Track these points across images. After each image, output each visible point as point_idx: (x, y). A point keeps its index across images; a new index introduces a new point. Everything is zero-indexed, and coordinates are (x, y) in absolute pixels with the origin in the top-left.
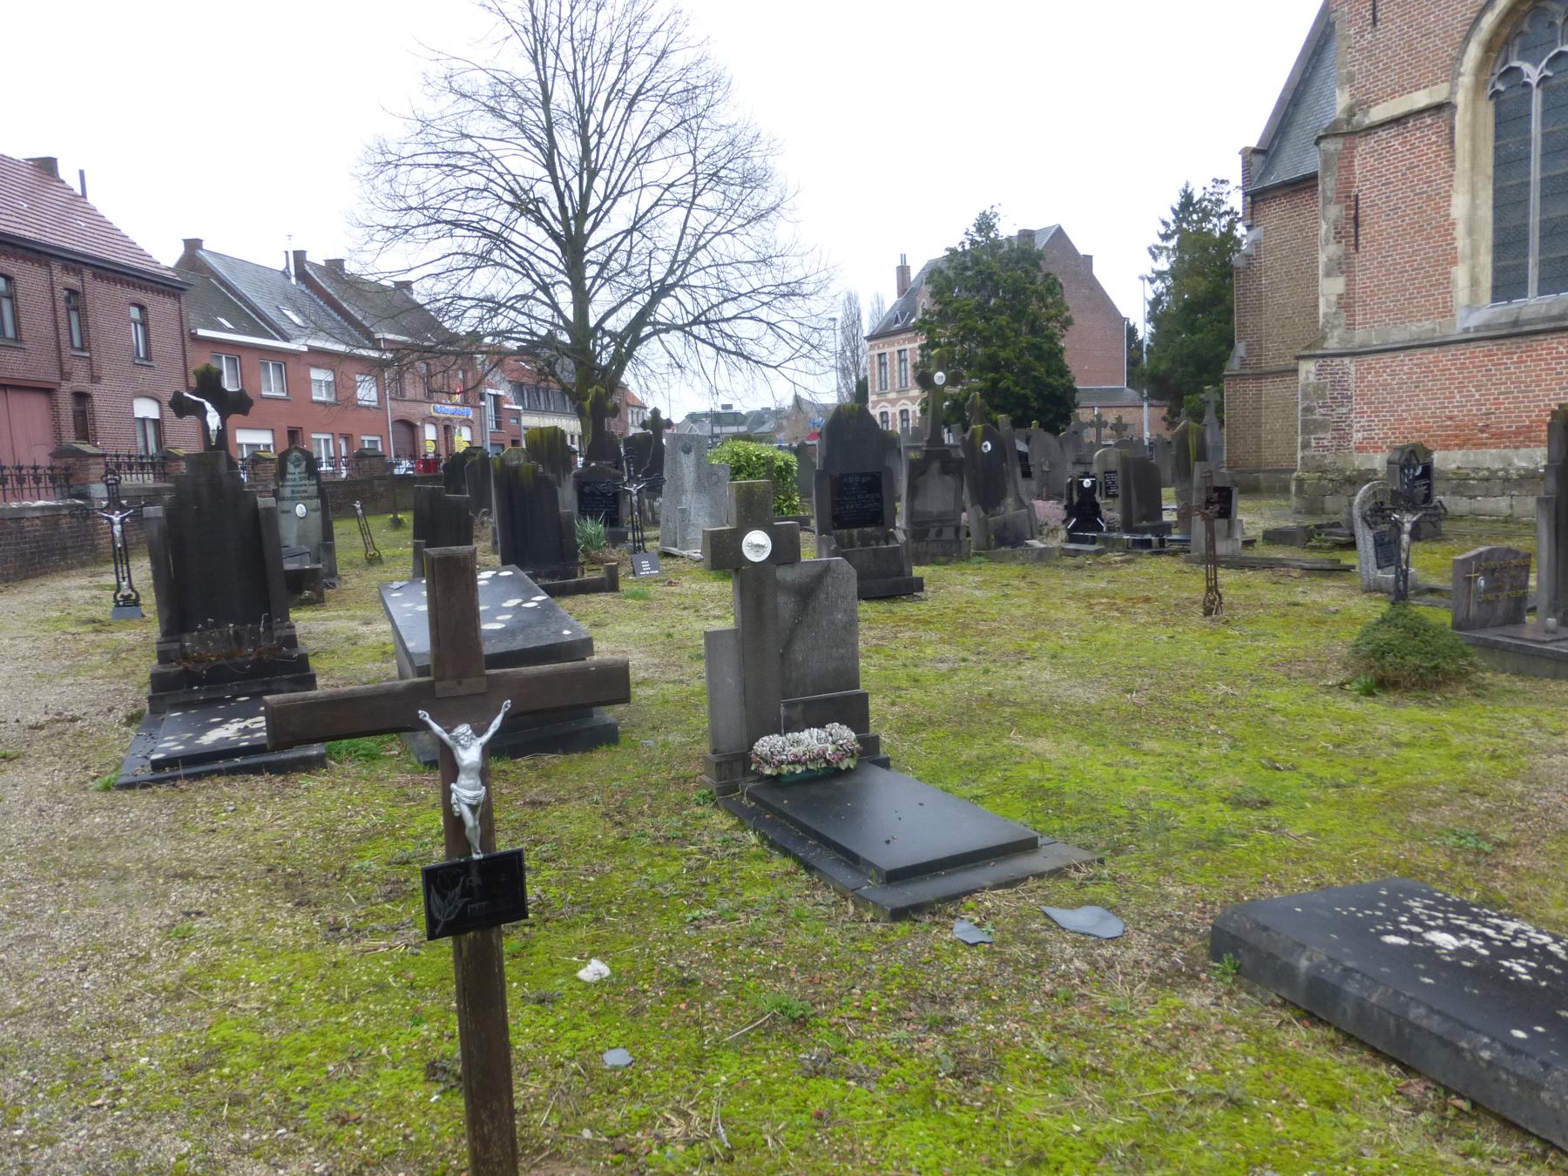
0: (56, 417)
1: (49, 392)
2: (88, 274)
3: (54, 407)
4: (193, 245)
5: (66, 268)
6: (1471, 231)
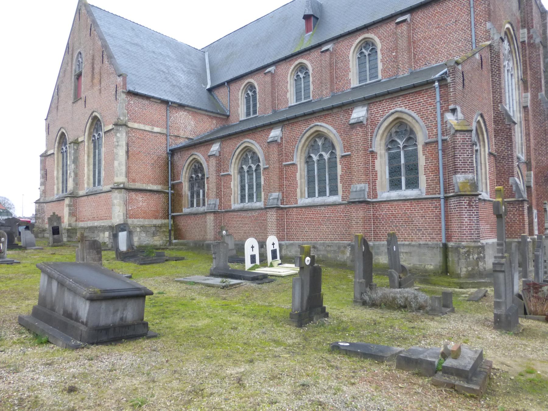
6: (57, 179)
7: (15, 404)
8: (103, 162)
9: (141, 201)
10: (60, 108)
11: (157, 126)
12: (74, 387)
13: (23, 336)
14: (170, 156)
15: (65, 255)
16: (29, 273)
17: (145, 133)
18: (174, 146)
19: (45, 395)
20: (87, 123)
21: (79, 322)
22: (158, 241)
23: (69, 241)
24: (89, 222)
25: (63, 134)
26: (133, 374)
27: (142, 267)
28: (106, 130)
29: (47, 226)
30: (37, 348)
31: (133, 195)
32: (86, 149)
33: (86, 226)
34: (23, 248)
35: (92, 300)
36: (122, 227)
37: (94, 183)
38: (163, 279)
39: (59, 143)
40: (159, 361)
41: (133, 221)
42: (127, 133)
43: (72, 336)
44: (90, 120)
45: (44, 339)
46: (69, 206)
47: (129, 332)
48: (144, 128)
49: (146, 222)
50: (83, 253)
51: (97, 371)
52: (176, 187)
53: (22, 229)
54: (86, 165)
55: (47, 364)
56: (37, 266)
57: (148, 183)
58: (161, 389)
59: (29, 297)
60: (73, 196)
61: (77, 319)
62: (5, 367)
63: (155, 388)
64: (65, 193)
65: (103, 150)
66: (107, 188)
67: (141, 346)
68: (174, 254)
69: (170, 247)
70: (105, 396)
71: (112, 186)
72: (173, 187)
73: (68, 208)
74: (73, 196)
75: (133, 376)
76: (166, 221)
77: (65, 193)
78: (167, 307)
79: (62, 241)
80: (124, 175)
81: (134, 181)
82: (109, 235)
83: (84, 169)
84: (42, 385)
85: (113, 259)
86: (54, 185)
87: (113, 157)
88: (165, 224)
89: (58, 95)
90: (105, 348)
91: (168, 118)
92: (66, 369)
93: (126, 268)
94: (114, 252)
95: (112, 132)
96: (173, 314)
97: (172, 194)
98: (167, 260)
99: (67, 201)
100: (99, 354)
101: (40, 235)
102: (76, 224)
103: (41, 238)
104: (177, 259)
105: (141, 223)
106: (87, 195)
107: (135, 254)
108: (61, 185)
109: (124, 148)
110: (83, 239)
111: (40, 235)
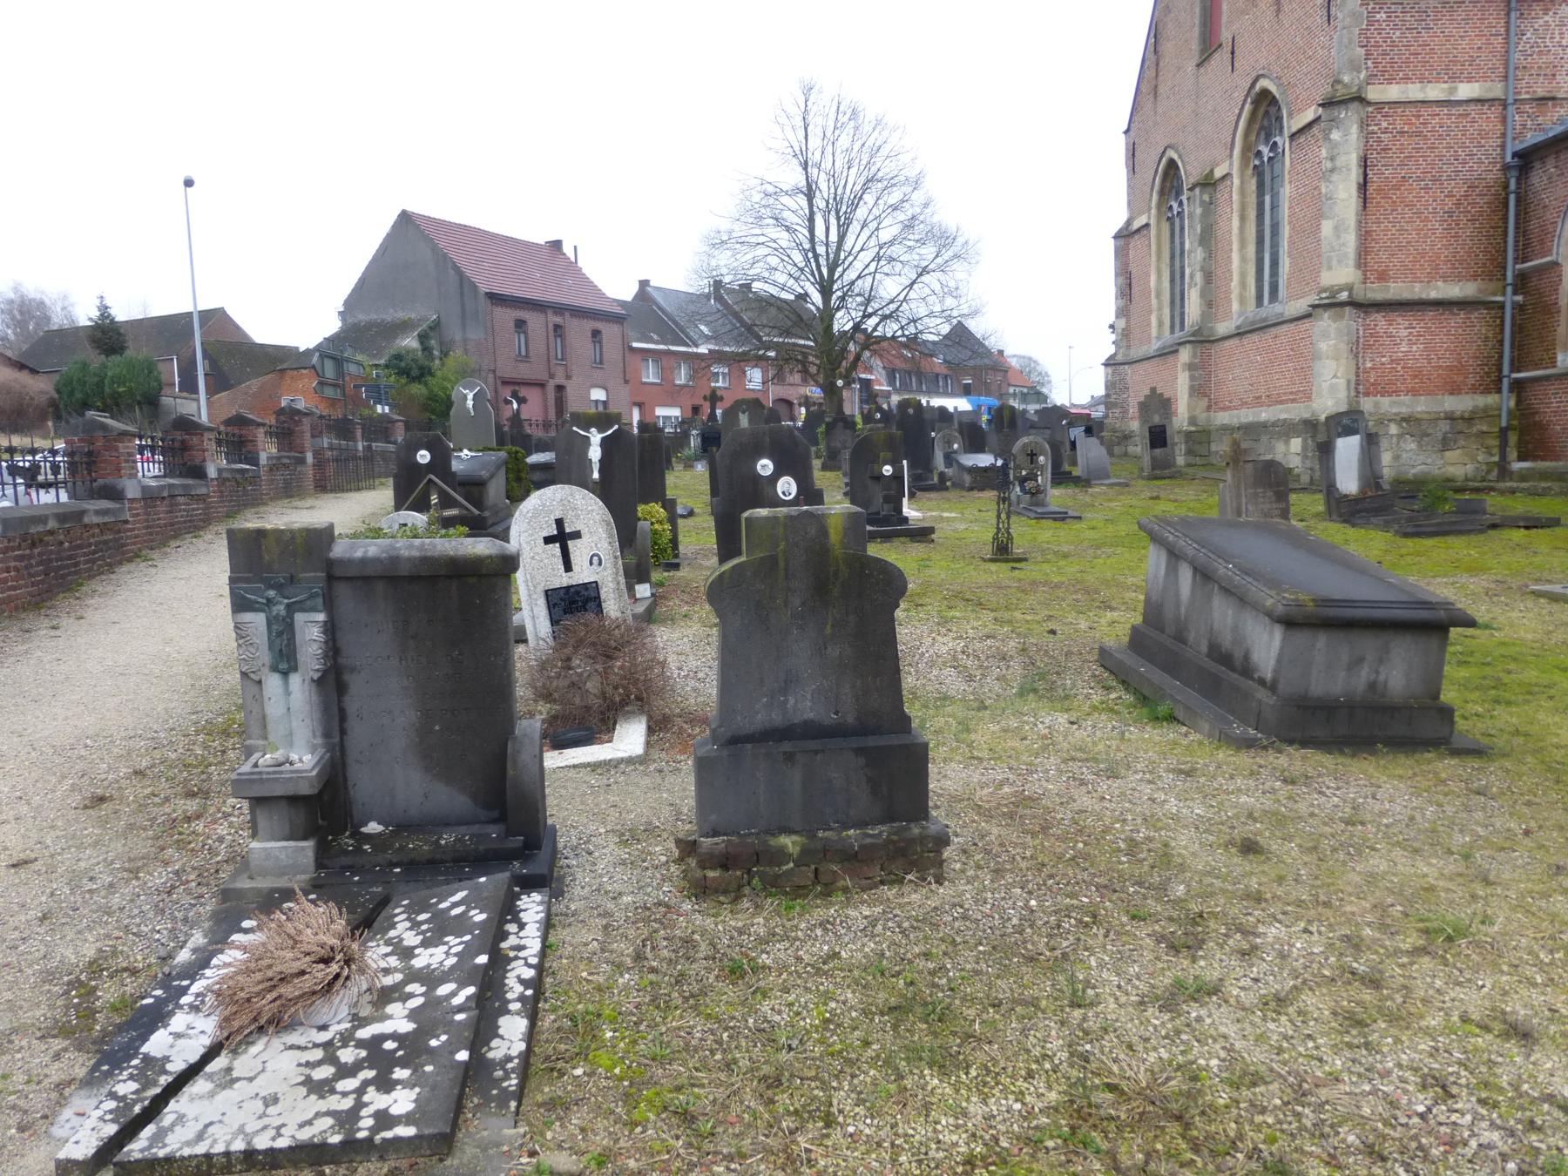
0: (545, 400)
1: (542, 385)
2: (567, 314)
3: (544, 394)
4: (644, 284)
5: (555, 313)
6: (1158, 296)
7: (1119, 850)
8: (1286, 231)
9: (1405, 340)
10: (1161, 89)
11: (1470, 79)
12: (1256, 843)
13: (1113, 696)
14: (1515, 173)
15: (1185, 501)
16: (1104, 544)
17: (1425, 112)
18: (1532, 138)
19: (1184, 842)
20: (1239, 116)
21: (1252, 679)
22: (1458, 464)
23: (1189, 465)
24: (1244, 411)
25: (1172, 164)
26: (1416, 845)
27: (1411, 544)
28: (1294, 130)
29: (1135, 425)
30: (1148, 728)
31: (1379, 321)
32: (1235, 197)
33: (1235, 422)
34: (1083, 482)
35: (1290, 623)
36: (1345, 421)
37: (1259, 297)
38: (1484, 583)
39: (1162, 193)
40: (1498, 825)
41: (1376, 405)
42: (1363, 125)
43: (1233, 713)
44: (1248, 107)
45: (1162, 709)
46: (1191, 367)
47: (1403, 726)
48: (1420, 96)
49: (1421, 406)
50: (1239, 496)
51: (1312, 815)
52: (1534, 282)
53: (1077, 433)
54: (1235, 247)
55: (1181, 772)
56: (1141, 526)
57: (1431, 279)
58: (1513, 909)
59: (1114, 604)
60: (1202, 340)
61: (1247, 670)
62: (1087, 760)
63: (1495, 902)
64: (1178, 334)
65: (1287, 191)
66: (1300, 306)
67: (1436, 774)
68: (1519, 506)
69: (1501, 485)
70: (1341, 884)
71: (1313, 299)
72: (1522, 282)
73: (1187, 373)
74: (1202, 340)
75: (1416, 851)
76: (1491, 399)
77: (1178, 334)
78: (1509, 672)
79: (1174, 465)
80: (1351, 262)
81: (1383, 277)
82: (1305, 448)
83: (1230, 257)
84: (1175, 818)
85: (1317, 515)
86: (1150, 313)
87: (1316, 206)
88: (1486, 409)
89: (1156, 52)
90: (1327, 760)
91: (1514, 39)
92: (1227, 792)
93: (1368, 544)
94: (1320, 496)
95: (1315, 130)
96: (1530, 693)
97: (1515, 305)
98: (1494, 526)
99: (1185, 355)
100: (1311, 772)
101: (1117, 450)
102: (1208, 420)
103: (1119, 457)
104: (1532, 524)
105: (1404, 410)
106: (1239, 334)
107: (1380, 503)
108: (1167, 311)
109: (1354, 175)
110: (1237, 457)
111: (1117, 450)
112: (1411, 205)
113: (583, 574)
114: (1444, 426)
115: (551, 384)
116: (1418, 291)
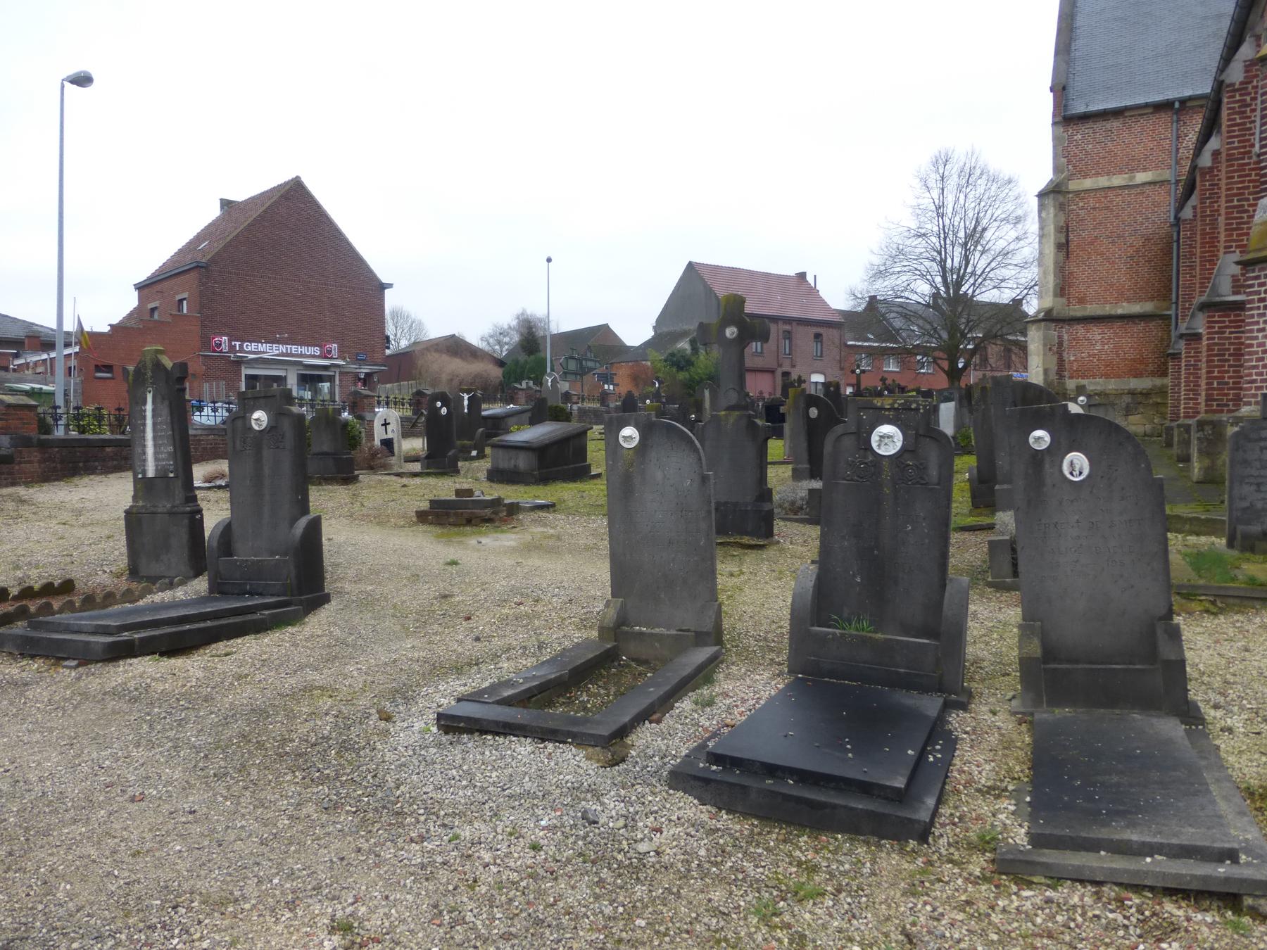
1: (772, 372)
3: (774, 378)
9: (1098, 341)
11: (1145, 170)
17: (1111, 195)
36: (946, 394)
48: (1107, 184)
49: (1112, 385)
57: (1117, 301)
112: (1102, 254)
113: (390, 435)
114: (1127, 399)
115: (780, 371)
116: (1108, 309)
